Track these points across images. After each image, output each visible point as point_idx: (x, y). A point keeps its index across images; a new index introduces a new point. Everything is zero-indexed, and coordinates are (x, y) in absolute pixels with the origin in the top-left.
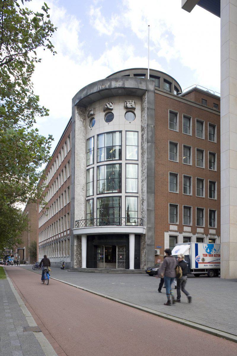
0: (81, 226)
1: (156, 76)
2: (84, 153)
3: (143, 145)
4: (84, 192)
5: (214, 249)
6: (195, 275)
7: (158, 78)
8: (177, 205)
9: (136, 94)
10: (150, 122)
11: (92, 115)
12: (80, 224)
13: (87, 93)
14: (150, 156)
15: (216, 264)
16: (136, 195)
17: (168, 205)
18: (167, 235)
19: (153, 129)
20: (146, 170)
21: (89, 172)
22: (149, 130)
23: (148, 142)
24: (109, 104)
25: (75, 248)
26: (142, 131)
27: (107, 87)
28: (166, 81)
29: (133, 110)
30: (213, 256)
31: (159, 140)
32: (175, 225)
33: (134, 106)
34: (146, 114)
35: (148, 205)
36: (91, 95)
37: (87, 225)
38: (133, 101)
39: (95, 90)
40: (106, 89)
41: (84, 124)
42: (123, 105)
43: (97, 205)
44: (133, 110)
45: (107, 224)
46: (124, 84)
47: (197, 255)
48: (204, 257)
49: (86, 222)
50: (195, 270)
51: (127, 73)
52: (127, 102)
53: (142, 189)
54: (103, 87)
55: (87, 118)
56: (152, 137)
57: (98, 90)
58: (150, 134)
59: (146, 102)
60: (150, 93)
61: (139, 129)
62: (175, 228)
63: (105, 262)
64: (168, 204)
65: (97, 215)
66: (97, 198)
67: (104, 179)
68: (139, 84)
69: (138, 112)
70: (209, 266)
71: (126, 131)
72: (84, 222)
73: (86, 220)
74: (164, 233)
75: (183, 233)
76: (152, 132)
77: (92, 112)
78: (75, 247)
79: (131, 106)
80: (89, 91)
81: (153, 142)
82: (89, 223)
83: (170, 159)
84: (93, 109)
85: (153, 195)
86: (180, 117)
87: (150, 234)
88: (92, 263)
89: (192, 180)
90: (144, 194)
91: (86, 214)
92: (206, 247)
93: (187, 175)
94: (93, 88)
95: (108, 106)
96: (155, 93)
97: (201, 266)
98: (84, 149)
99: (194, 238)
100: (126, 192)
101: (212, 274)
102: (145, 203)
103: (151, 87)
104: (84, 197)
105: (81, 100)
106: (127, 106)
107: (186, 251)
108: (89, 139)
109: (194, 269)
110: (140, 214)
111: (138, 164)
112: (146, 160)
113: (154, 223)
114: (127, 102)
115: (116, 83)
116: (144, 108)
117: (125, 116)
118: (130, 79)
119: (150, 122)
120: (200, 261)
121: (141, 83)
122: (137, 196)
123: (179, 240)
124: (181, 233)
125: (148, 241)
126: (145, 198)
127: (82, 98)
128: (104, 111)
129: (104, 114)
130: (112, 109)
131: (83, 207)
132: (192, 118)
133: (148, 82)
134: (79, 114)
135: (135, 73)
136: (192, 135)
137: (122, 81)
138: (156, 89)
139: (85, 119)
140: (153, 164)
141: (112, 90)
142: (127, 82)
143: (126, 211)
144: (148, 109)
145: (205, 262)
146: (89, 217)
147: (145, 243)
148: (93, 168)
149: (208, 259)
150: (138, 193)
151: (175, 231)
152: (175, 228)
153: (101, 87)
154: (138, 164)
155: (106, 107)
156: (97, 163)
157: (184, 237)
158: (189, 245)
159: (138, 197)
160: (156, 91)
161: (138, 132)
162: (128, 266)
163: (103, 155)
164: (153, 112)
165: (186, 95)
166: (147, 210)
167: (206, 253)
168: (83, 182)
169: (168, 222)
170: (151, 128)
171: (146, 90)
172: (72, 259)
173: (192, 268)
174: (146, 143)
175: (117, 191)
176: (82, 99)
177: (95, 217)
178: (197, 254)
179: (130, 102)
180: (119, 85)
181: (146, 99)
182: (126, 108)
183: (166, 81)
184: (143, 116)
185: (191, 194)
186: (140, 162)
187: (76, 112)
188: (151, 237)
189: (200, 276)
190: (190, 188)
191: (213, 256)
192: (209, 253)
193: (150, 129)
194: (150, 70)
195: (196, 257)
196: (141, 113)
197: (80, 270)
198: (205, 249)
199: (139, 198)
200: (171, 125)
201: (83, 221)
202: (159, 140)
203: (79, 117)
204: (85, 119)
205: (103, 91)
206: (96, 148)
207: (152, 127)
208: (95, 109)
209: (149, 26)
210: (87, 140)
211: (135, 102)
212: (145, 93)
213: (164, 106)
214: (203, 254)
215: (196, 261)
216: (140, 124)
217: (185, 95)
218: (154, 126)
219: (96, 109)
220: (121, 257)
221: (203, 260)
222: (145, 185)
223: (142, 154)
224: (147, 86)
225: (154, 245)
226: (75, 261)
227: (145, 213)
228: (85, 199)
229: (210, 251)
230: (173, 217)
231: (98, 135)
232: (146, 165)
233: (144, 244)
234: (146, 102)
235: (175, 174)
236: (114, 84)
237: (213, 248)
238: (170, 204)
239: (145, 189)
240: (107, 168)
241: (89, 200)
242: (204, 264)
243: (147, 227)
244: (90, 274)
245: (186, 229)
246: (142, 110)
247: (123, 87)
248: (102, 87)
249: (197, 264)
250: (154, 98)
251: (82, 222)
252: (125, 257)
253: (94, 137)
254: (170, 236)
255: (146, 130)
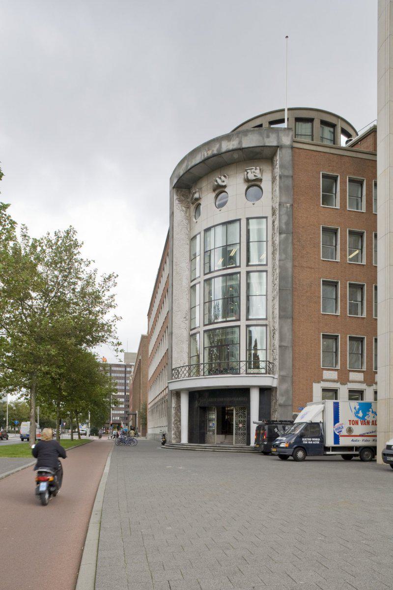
0: (183, 375)
1: (303, 117)
2: (188, 261)
3: (274, 239)
4: (187, 322)
5: (373, 412)
6: (343, 456)
7: (311, 120)
8: (337, 336)
9: (262, 156)
10: (284, 199)
11: (197, 199)
12: (181, 373)
13: (187, 166)
14: (284, 256)
15: (365, 438)
16: (264, 322)
17: (346, 338)
18: (317, 388)
19: (289, 210)
20: (278, 280)
21: (195, 290)
22: (282, 213)
23: (280, 234)
24: (220, 178)
25: (173, 412)
26: (273, 215)
27: (215, 152)
28: (324, 123)
29: (258, 183)
30: (371, 423)
31: (303, 227)
32: (332, 370)
33: (259, 176)
34: (278, 187)
35: (281, 339)
36: (193, 168)
37: (192, 374)
38: (258, 168)
39: (198, 159)
40: (214, 156)
41: (187, 215)
42: (243, 177)
43: (201, 341)
44: (258, 183)
45: (221, 372)
46: (240, 142)
47: (338, 422)
48: (351, 426)
49: (189, 369)
50: (334, 449)
51: (258, 122)
52: (248, 171)
53: (273, 312)
54: (210, 153)
55: (191, 205)
56: (287, 224)
57: (203, 158)
58: (285, 218)
59: (278, 166)
60: (284, 151)
61: (269, 213)
62: (334, 375)
63: (217, 434)
64: (320, 334)
65: (204, 358)
66: (205, 331)
67: (214, 300)
68: (265, 139)
69: (266, 185)
70: (360, 442)
71: (248, 219)
72: (187, 369)
73: (190, 366)
74: (312, 385)
75: (348, 383)
76: (288, 215)
77: (197, 195)
78: (173, 410)
79: (255, 176)
80: (190, 163)
81: (291, 232)
82: (194, 371)
83: (323, 257)
84: (197, 190)
85: (290, 321)
86: (343, 183)
87: (284, 387)
88: (198, 434)
89: (365, 289)
90: (276, 321)
91: (190, 357)
92: (355, 408)
93: (356, 281)
94: (195, 157)
95: (219, 181)
96: (292, 148)
97: (344, 442)
98: (187, 255)
99: (343, 392)
100: (248, 319)
101: (367, 455)
102: (277, 336)
103: (286, 140)
104: (188, 329)
105: (180, 179)
106: (247, 177)
107: (317, 415)
108: (195, 237)
109: (332, 447)
110: (270, 354)
111: (266, 271)
112: (277, 263)
113: (291, 367)
114: (248, 171)
115: (228, 143)
116: (276, 177)
117: (246, 197)
118: (250, 133)
119: (284, 199)
120: (344, 432)
121: (268, 137)
122: (265, 323)
123: (341, 397)
124: (343, 384)
125: (280, 399)
126: (277, 326)
127: (181, 175)
128: (214, 191)
129: (214, 195)
130: (225, 187)
131: (185, 346)
132: (365, 181)
133: (280, 133)
134: (180, 201)
135: (271, 120)
136: (366, 210)
137: (237, 139)
138: (294, 141)
139: (188, 208)
140: (290, 270)
141: (223, 155)
142: (246, 138)
143: (247, 350)
144: (280, 177)
145: (353, 434)
146: (194, 361)
147: (276, 401)
148: (200, 282)
149: (359, 429)
150: (266, 319)
151: (334, 381)
152: (334, 375)
153: (206, 154)
154: (266, 271)
155: (216, 183)
156: (205, 274)
157: (351, 392)
158: (323, 406)
159: (266, 325)
160: (296, 145)
161: (266, 218)
162: (248, 443)
163: (217, 262)
164: (289, 182)
165: (360, 141)
166: (280, 346)
167: (356, 419)
168: (186, 306)
169: (320, 366)
170: (285, 209)
171: (278, 147)
172: (169, 430)
173: (327, 445)
174: (278, 234)
175: (234, 318)
176: (181, 177)
177: (201, 361)
178: (336, 420)
179: (253, 170)
180: (233, 145)
181: (278, 162)
182: (247, 180)
183: (324, 123)
184: (274, 190)
185: (365, 315)
186: (269, 268)
187: (175, 197)
188: (287, 391)
189: (354, 458)
190: (362, 305)
191: (371, 423)
192: (363, 418)
193: (284, 210)
194: (289, 109)
195: (336, 425)
196: (272, 185)
197: (178, 447)
198: (354, 411)
199: (268, 327)
200: (327, 200)
201: (185, 367)
202: (303, 227)
203: (179, 205)
204: (188, 208)
205: (209, 160)
206: (203, 252)
207: (287, 207)
208: (201, 189)
209: (287, 37)
210: (192, 239)
211: (260, 170)
212: (275, 154)
213: (313, 167)
214: (350, 421)
215: (334, 433)
216: (271, 204)
217: (358, 143)
218: (292, 205)
219: (203, 189)
220: (241, 425)
221: (350, 430)
222: (277, 306)
223: (273, 253)
224: (278, 138)
225: (292, 405)
226: (173, 432)
227: (277, 351)
228: (189, 333)
229: (365, 414)
230: (332, 353)
231: (207, 230)
232: (278, 271)
233: (275, 403)
234: (278, 166)
235: (332, 282)
236: (226, 146)
237: (370, 410)
238: (323, 335)
239: (277, 312)
240: (223, 282)
241: (195, 334)
242: (351, 438)
243: (279, 376)
244: (192, 453)
245: (353, 376)
246: (274, 179)
247: (239, 147)
248: (207, 154)
249: (336, 438)
250: (291, 157)
251: (183, 369)
252: (246, 426)
253: (200, 233)
254: (324, 390)
255: (277, 212)
